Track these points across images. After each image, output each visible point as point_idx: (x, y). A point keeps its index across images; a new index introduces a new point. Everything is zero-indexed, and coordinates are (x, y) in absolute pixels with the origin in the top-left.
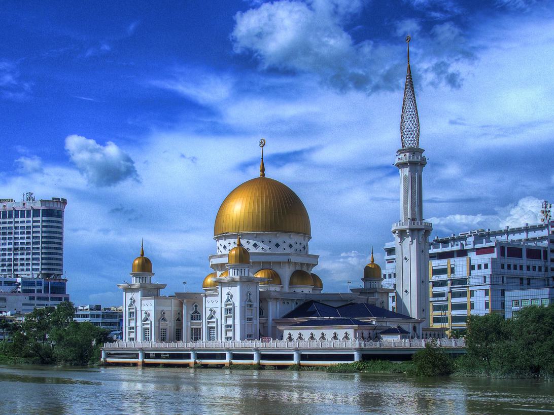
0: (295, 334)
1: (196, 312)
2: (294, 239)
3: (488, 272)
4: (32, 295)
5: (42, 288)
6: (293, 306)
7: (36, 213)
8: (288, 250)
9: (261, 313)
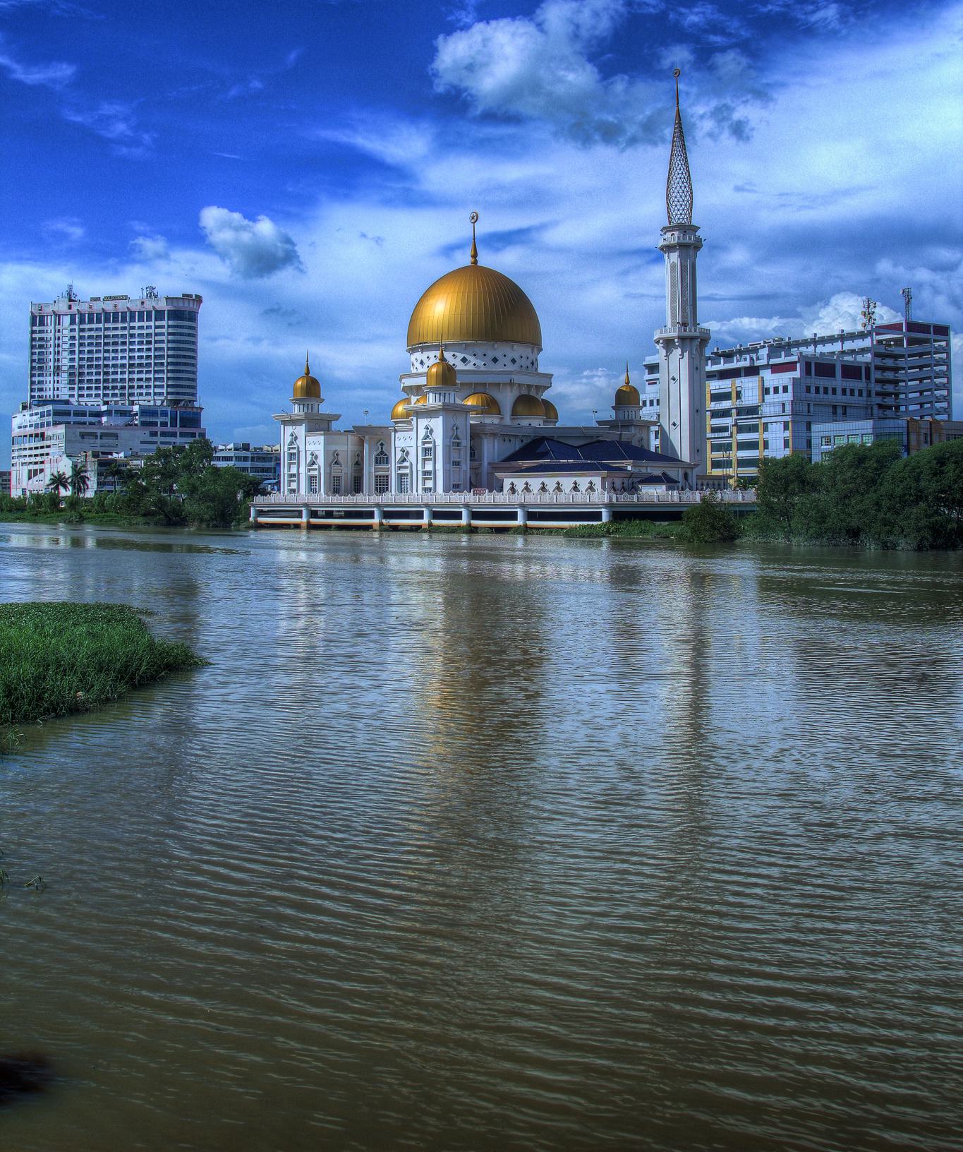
0: (520, 483)
1: (382, 452)
2: (518, 351)
3: (788, 397)
4: (154, 429)
5: (168, 420)
6: (517, 445)
7: (160, 315)
8: (510, 367)
9: (472, 455)
